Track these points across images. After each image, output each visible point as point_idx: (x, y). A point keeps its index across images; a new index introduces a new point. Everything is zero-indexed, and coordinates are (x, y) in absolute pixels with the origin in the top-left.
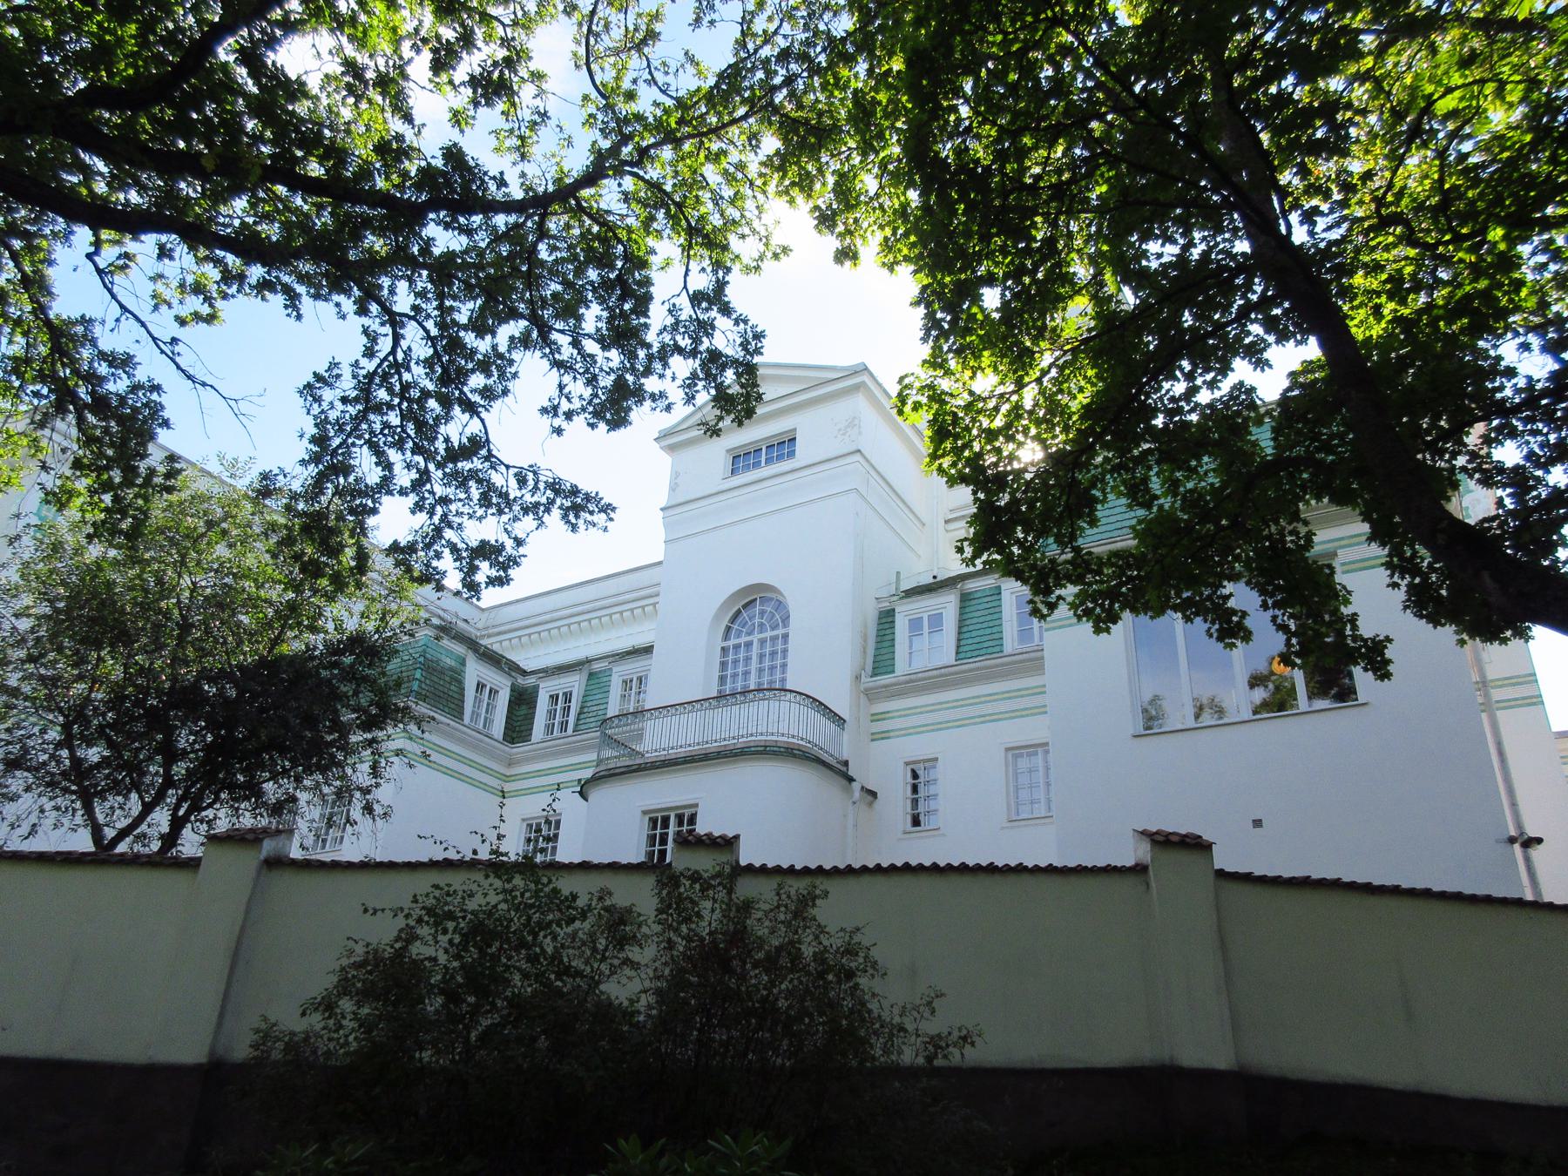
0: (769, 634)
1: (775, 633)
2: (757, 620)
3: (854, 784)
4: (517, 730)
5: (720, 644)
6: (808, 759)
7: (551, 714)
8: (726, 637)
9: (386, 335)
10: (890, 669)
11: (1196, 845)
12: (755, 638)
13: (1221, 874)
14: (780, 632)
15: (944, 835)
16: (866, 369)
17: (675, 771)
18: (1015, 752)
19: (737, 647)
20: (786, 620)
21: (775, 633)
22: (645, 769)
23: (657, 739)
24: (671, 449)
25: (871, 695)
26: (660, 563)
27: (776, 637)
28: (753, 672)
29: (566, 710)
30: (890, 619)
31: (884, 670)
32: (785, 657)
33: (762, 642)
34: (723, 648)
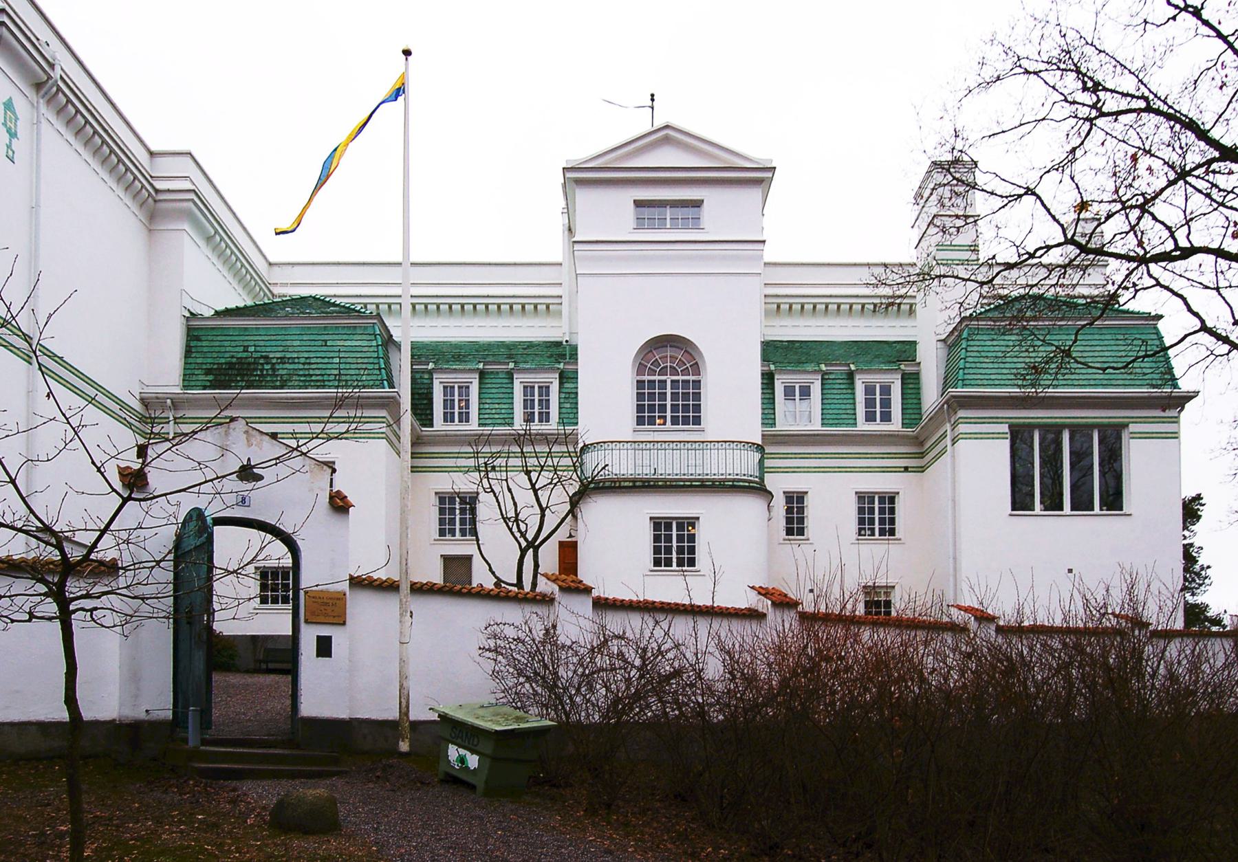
20: (696, 369)
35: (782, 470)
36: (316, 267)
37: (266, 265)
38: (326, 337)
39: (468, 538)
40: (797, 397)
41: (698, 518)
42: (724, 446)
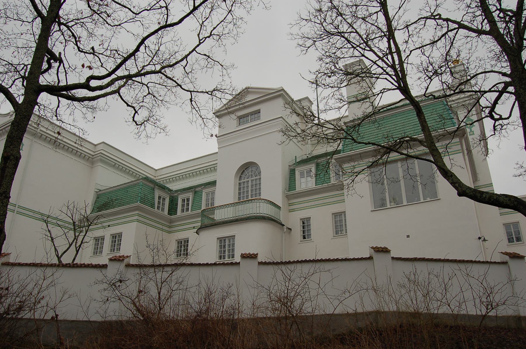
0: (255, 178)
1: (256, 178)
2: (250, 173)
3: (284, 226)
4: (173, 210)
5: (238, 182)
6: (270, 220)
7: (183, 206)
8: (240, 179)
9: (118, 82)
10: (294, 189)
11: (385, 251)
12: (250, 179)
13: (393, 258)
14: (258, 177)
15: (313, 242)
16: (283, 89)
17: (226, 225)
18: (335, 215)
19: (244, 182)
20: (260, 173)
21: (256, 178)
22: (217, 225)
23: (219, 215)
24: (218, 117)
25: (288, 197)
26: (217, 153)
27: (257, 179)
28: (250, 190)
29: (188, 204)
30: (294, 172)
31: (292, 189)
32: (260, 186)
33: (252, 181)
34: (239, 183)
35: (299, 209)
36: (169, 168)
37: (155, 171)
38: (127, 190)
39: (231, 259)
40: (305, 176)
41: (235, 236)
42: (259, 201)
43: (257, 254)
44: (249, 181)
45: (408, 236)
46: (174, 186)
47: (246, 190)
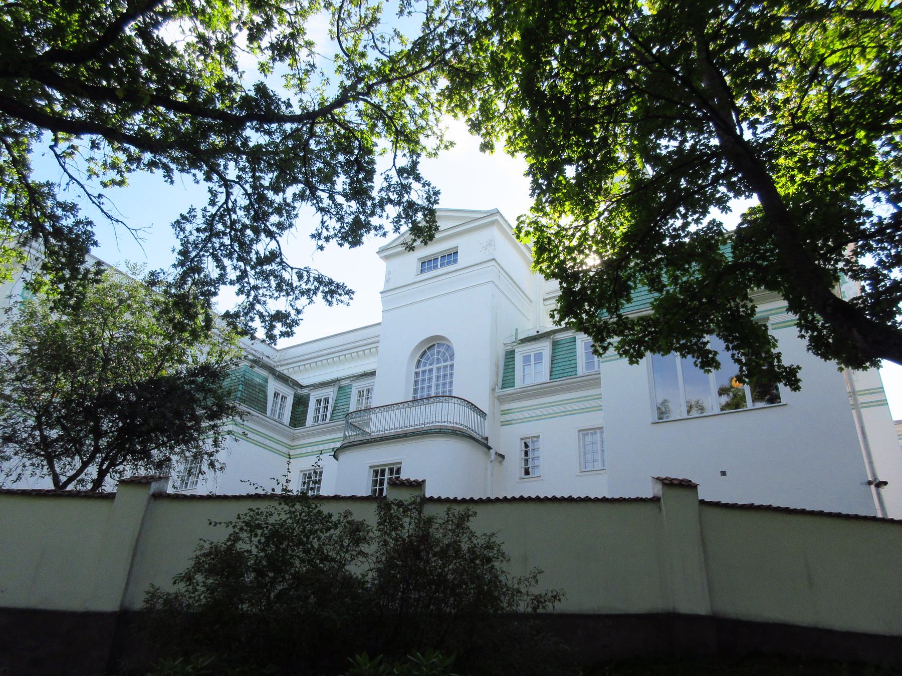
0: (442, 364)
1: (446, 364)
2: (435, 357)
3: (491, 451)
4: (298, 420)
5: (414, 370)
6: (465, 436)
7: (317, 410)
8: (418, 366)
10: (512, 385)
11: (688, 486)
12: (434, 367)
13: (702, 502)
14: (449, 363)
15: (543, 480)
16: (498, 212)
17: (388, 443)
18: (584, 432)
19: (424, 372)
20: (452, 356)
21: (446, 364)
22: (371, 442)
24: (386, 258)
25: (501, 399)
26: (380, 324)
27: (447, 366)
28: (433, 386)
29: (326, 408)
30: (512, 356)
31: (509, 385)
32: (451, 378)
33: (439, 369)
34: (416, 373)
43: (424, 481)
44: (431, 371)
45: (723, 473)
46: (305, 379)
47: (426, 385)
